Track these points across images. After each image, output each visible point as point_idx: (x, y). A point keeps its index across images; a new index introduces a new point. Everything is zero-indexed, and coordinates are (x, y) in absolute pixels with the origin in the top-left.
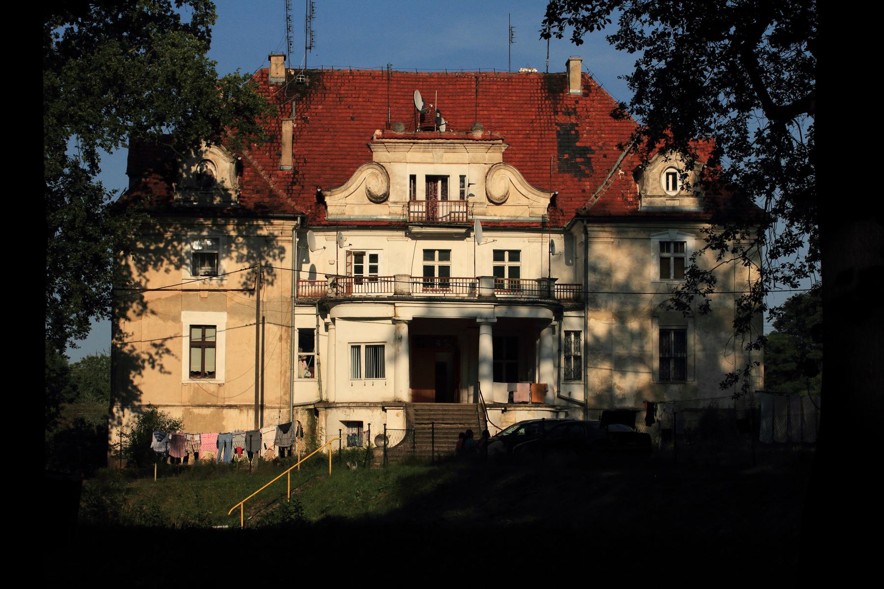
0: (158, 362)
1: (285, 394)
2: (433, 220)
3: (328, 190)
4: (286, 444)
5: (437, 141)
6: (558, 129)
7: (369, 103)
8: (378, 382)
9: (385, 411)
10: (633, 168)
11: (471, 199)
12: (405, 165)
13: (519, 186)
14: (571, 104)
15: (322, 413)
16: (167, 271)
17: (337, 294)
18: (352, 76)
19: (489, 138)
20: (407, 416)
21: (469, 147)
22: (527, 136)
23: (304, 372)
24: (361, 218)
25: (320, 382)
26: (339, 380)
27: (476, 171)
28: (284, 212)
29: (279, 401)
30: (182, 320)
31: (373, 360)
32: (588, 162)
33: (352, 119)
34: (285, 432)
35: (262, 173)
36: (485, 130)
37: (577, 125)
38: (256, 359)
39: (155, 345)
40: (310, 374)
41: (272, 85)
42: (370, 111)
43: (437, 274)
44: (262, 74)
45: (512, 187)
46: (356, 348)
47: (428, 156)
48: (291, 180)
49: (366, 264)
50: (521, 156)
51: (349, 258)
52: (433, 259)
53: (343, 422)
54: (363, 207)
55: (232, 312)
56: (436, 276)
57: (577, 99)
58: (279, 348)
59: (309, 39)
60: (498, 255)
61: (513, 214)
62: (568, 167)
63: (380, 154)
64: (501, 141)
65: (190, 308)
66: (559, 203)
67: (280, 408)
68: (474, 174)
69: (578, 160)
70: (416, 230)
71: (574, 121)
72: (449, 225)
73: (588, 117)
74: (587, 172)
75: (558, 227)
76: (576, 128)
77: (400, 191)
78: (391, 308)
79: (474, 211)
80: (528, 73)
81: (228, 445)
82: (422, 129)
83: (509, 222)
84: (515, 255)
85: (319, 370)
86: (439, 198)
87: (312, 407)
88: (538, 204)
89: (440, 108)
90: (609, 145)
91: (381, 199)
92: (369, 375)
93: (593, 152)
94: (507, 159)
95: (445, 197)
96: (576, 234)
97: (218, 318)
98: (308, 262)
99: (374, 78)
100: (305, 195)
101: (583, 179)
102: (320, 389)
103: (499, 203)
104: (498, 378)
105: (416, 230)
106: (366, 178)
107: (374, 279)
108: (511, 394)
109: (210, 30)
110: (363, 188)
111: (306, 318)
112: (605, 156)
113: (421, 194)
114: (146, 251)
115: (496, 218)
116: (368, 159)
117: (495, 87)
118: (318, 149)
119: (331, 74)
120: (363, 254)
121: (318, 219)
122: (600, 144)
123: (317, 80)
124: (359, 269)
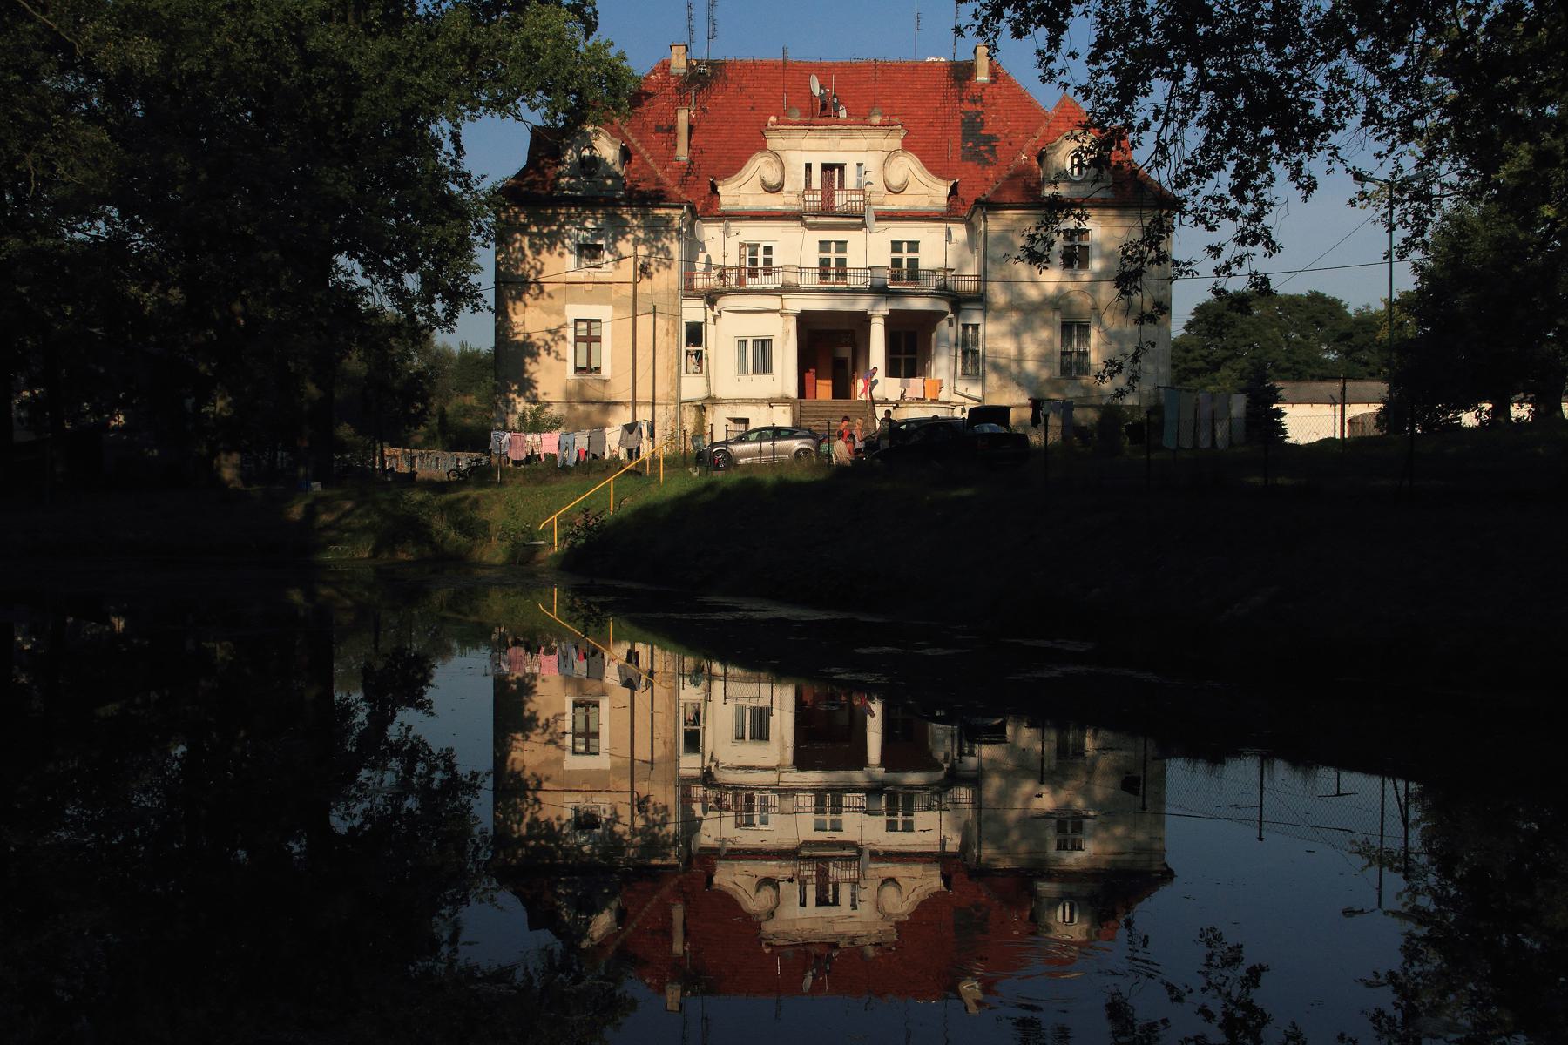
2: (828, 209)
4: (633, 446)
8: (766, 377)
11: (869, 188)
12: (800, 152)
16: (561, 255)
18: (755, 67)
21: (866, 133)
22: (931, 124)
23: (692, 368)
25: (708, 378)
26: (726, 374)
27: (874, 159)
32: (993, 150)
39: (550, 331)
47: (824, 143)
49: (761, 257)
55: (617, 306)
57: (983, 87)
58: (671, 344)
60: (896, 246)
62: (974, 156)
63: (774, 141)
65: (574, 302)
68: (872, 161)
70: (810, 220)
71: (979, 108)
77: (795, 181)
82: (821, 114)
84: (914, 246)
88: (937, 193)
89: (835, 99)
91: (776, 189)
94: (907, 146)
95: (841, 186)
97: (602, 311)
102: (709, 385)
104: (892, 371)
105: (810, 220)
106: (759, 167)
107: (768, 272)
108: (646, 403)
110: (757, 177)
111: (694, 311)
113: (817, 183)
114: (540, 234)
116: (762, 146)
124: (754, 262)
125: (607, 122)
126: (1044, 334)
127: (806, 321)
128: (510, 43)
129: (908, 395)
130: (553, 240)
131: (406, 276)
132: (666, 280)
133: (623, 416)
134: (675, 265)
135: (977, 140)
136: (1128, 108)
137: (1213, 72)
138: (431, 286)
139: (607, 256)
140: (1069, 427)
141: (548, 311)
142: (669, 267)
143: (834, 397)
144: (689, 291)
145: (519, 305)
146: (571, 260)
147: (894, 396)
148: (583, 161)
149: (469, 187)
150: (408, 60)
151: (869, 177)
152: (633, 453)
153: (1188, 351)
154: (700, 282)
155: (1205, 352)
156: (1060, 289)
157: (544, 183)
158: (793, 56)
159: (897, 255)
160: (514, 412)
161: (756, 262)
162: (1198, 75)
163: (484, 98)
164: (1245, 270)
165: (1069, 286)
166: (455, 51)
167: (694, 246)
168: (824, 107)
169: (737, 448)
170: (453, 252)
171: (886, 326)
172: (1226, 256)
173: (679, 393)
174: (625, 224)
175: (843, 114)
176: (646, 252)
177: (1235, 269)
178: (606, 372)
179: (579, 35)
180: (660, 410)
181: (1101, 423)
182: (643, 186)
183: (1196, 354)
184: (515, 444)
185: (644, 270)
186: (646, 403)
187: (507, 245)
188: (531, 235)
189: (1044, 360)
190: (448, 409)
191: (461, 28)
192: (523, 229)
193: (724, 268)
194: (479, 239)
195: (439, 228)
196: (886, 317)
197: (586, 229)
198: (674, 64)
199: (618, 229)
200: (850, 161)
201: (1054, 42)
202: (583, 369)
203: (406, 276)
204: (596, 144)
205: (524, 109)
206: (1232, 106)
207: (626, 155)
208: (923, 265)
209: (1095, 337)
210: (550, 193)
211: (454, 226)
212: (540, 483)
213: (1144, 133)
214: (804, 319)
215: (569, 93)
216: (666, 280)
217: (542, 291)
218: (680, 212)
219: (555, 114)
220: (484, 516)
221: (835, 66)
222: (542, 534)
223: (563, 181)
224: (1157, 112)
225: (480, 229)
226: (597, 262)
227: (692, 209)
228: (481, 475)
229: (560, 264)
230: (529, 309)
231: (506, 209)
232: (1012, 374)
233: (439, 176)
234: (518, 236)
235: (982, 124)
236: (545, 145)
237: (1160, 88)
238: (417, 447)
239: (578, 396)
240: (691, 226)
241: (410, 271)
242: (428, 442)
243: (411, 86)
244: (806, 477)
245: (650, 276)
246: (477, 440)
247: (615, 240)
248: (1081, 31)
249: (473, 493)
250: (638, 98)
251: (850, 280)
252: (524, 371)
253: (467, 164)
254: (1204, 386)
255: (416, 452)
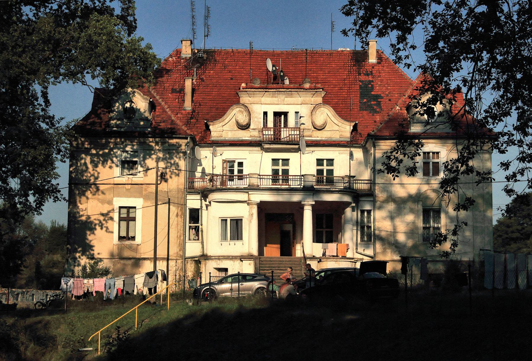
0: (105, 225)
1: (180, 251)
2: (277, 138)
3: (212, 122)
4: (152, 286)
5: (280, 90)
6: (361, 84)
7: (242, 70)
8: (238, 243)
9: (242, 261)
10: (405, 105)
11: (302, 127)
12: (262, 105)
13: (333, 119)
14: (369, 69)
15: (203, 263)
16: (111, 167)
17: (213, 186)
18: (233, 53)
19: (314, 88)
20: (255, 265)
22: (341, 89)
23: (192, 237)
24: (232, 139)
25: (202, 243)
26: (214, 242)
27: (302, 108)
28: (180, 134)
29: (175, 255)
30: (114, 203)
31: (234, 228)
32: (379, 104)
33: (232, 79)
34: (151, 278)
35: (168, 110)
36: (311, 83)
37: (373, 81)
38: (176, 227)
40: (197, 238)
41: (183, 59)
42: (243, 74)
43: (280, 174)
44: (177, 52)
45: (329, 119)
46: (224, 221)
47: (275, 100)
48: (190, 116)
50: (336, 101)
51: (225, 164)
52: (278, 165)
53: (215, 268)
54: (234, 132)
55: (146, 198)
56: (280, 175)
57: (373, 66)
59: (206, 30)
60: (320, 162)
61: (329, 136)
63: (245, 99)
64: (321, 90)
65: (119, 196)
66: (359, 128)
67: (177, 260)
68: (304, 111)
69: (372, 103)
72: (287, 143)
73: (380, 76)
74: (378, 110)
75: (357, 144)
76: (372, 83)
77: (257, 122)
78: (246, 195)
79: (305, 134)
80: (342, 51)
81: (112, 287)
82: (273, 82)
83: (324, 141)
84: (330, 162)
85: (202, 235)
86: (282, 126)
87: (197, 259)
88: (343, 129)
89: (285, 73)
90: (392, 93)
91: (245, 127)
92: (232, 238)
93: (382, 98)
94: (326, 101)
95: (286, 125)
96: (369, 148)
97: (137, 202)
98: (201, 165)
99: (246, 54)
100: (198, 125)
101: (375, 114)
102: (203, 247)
103: (321, 129)
106: (236, 114)
107: (241, 178)
108: (163, 259)
109: (136, 20)
110: (234, 120)
111: (194, 202)
112: (390, 100)
113: (270, 124)
114: (97, 155)
115: (318, 139)
116: (236, 101)
117: (322, 59)
118: (208, 97)
119: (220, 52)
120: (234, 161)
121: (205, 140)
122: (387, 93)
123: (212, 56)
124: (232, 171)
125: (140, 87)
126: (410, 218)
127: (263, 208)
128: (79, 38)
129: (327, 254)
130: (106, 158)
131: (10, 180)
132: (176, 183)
133: (148, 267)
134: (182, 174)
135: (369, 98)
136: (446, 79)
137: (499, 58)
138: (27, 186)
139: (140, 169)
140: (425, 274)
141: (103, 202)
142: (178, 175)
143: (282, 254)
144: (191, 189)
145: (83, 199)
146: (117, 171)
147: (319, 254)
148: (125, 110)
149: (53, 125)
150: (13, 47)
151: (303, 120)
152: (152, 290)
153: (508, 226)
154: (198, 184)
155: (520, 228)
156: (419, 190)
157: (101, 123)
158: (257, 47)
159: (320, 168)
160: (79, 265)
161: (233, 171)
162: (489, 59)
163: (62, 71)
164: (525, 178)
165: (425, 188)
166: (44, 42)
167: (194, 162)
168: (275, 78)
169: (219, 287)
170: (41, 166)
171: (258, 208)
172: (512, 169)
173: (184, 253)
174: (151, 149)
175: (287, 82)
176: (164, 166)
177: (519, 177)
178: (138, 240)
179: (124, 34)
180: (172, 263)
181: (447, 271)
182: (163, 125)
183: (514, 228)
184: (74, 286)
185: (163, 177)
186: (163, 259)
187: (77, 160)
188: (92, 155)
189: (411, 233)
190: (42, 263)
191: (48, 28)
192: (87, 152)
193: (213, 175)
194: (59, 157)
195: (32, 151)
196: (313, 206)
197: (127, 152)
198: (183, 51)
199: (148, 151)
200: (291, 110)
201: (402, 39)
202: (124, 237)
203: (10, 180)
204: (135, 99)
205: (88, 77)
206: (514, 77)
207: (152, 106)
208: (336, 173)
209: (443, 219)
210: (105, 129)
211: (42, 149)
212: (91, 310)
213: (457, 95)
214: (262, 206)
215: (116, 68)
216: (176, 183)
217: (98, 189)
218: (185, 141)
219: (108, 81)
220: (54, 332)
221: (282, 53)
222: (91, 344)
223: (113, 122)
224: (465, 81)
225: (59, 151)
226: (133, 172)
227: (193, 139)
228: (57, 306)
229: (110, 173)
230: (90, 201)
231: (76, 140)
232: (390, 242)
233: (33, 119)
234: (83, 156)
235: (373, 88)
236: (103, 100)
237: (467, 67)
238: (21, 287)
239: (118, 256)
240: (193, 149)
241: (13, 177)
242: (28, 285)
243: (16, 63)
244: (265, 306)
245: (166, 181)
246: (54, 283)
247: (144, 159)
248: (419, 34)
249: (48, 318)
250: (161, 72)
251: (290, 182)
252: (85, 238)
253: (51, 111)
254: (520, 249)
255: (20, 290)
